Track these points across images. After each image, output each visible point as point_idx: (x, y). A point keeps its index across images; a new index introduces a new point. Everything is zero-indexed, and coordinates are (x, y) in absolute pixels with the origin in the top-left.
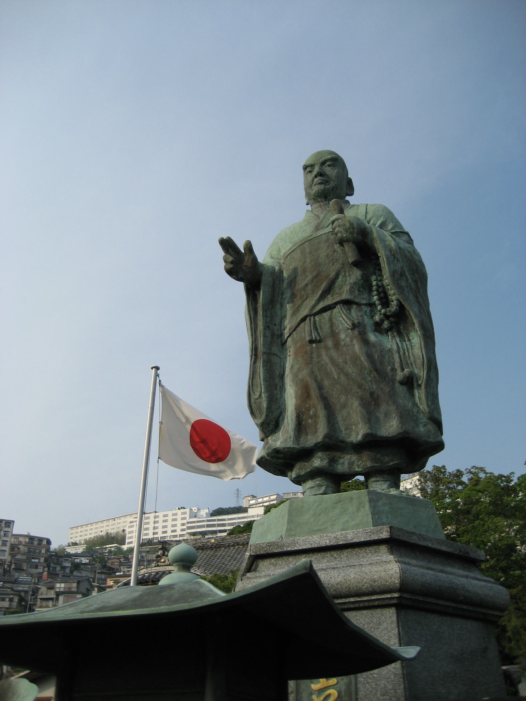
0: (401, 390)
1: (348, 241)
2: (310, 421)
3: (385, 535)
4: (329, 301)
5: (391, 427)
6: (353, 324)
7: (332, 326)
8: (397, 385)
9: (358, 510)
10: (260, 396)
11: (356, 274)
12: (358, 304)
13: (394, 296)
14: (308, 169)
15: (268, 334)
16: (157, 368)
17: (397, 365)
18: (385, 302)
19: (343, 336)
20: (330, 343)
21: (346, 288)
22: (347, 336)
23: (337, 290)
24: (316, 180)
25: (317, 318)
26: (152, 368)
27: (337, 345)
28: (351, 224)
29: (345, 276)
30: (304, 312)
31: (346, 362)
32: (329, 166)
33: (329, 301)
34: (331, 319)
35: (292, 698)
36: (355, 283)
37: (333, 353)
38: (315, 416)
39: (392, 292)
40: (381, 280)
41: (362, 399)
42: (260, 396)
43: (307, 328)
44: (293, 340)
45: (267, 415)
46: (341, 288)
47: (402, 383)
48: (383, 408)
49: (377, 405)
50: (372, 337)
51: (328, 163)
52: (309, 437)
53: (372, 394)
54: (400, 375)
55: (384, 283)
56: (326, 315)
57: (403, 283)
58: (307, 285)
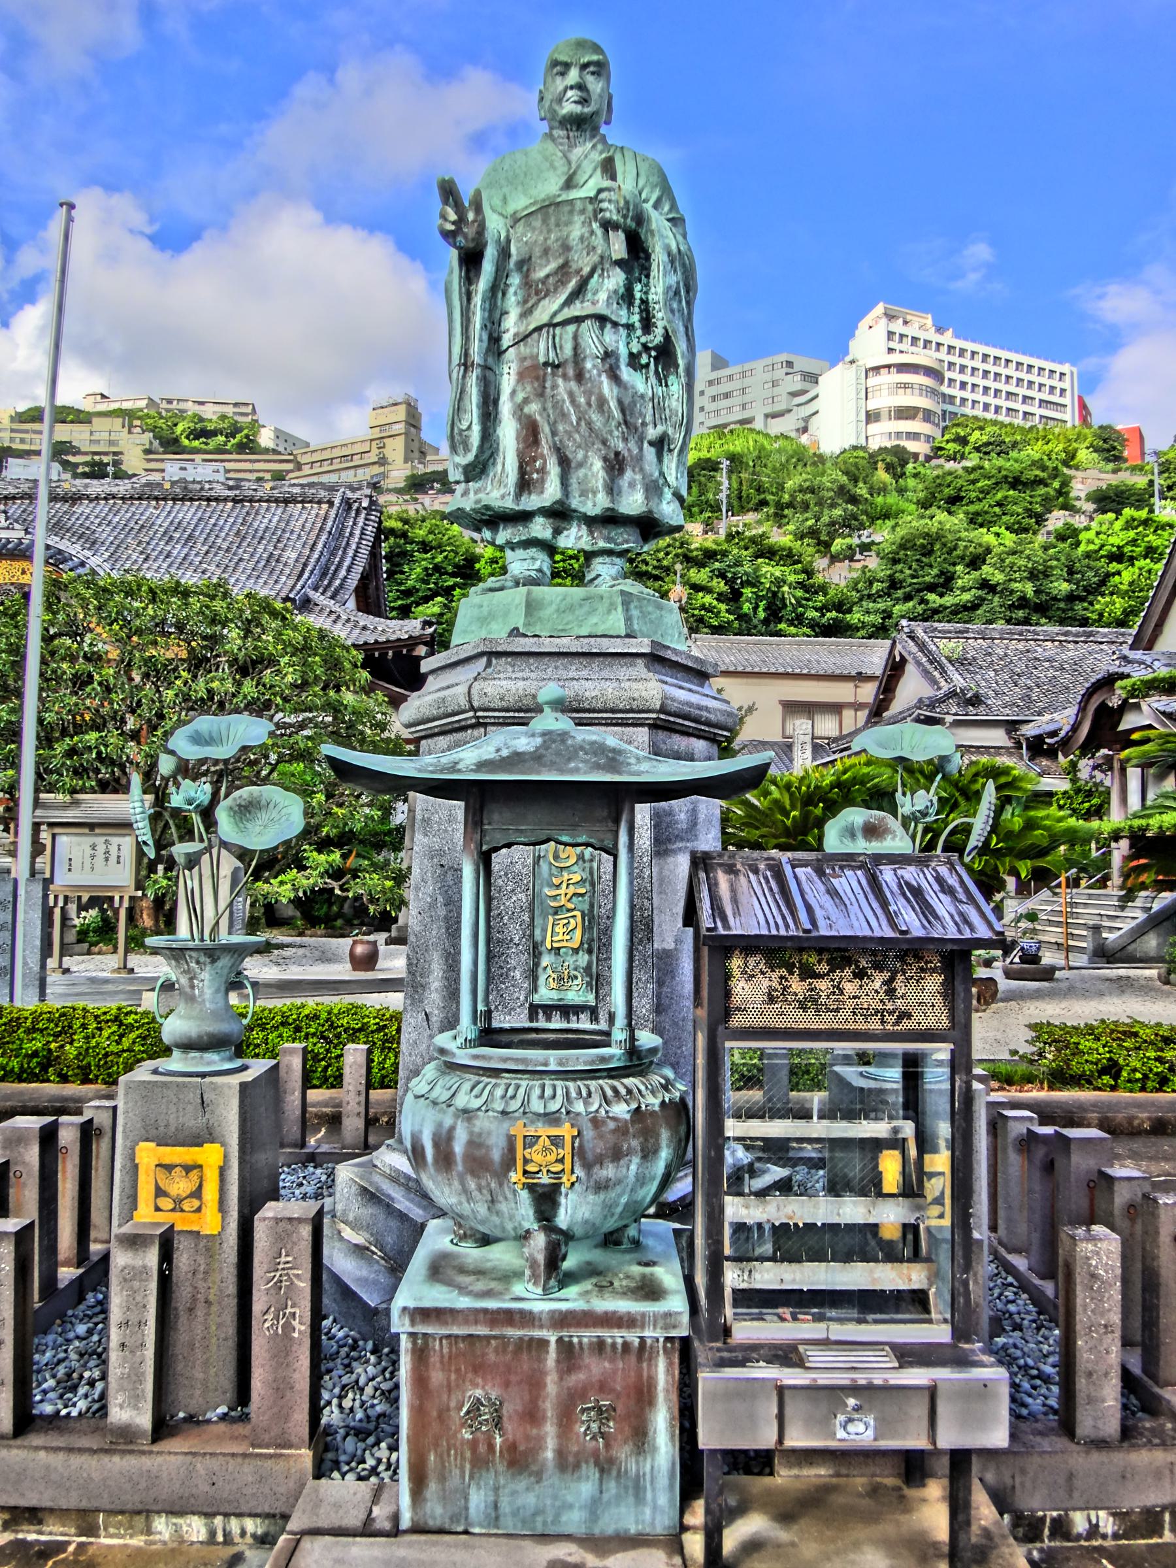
0: (650, 453)
1: (616, 226)
2: (535, 476)
3: (647, 650)
4: (576, 310)
5: (633, 503)
6: (606, 353)
7: (576, 348)
8: (646, 445)
9: (609, 612)
10: (469, 428)
11: (616, 279)
12: (615, 324)
13: (661, 318)
14: (558, 68)
15: (485, 337)
16: (72, 207)
17: (649, 418)
18: (647, 324)
19: (588, 365)
20: (571, 372)
21: (602, 296)
22: (594, 366)
23: (589, 296)
24: (570, 93)
25: (558, 330)
26: (61, 205)
27: (580, 377)
28: (627, 203)
29: (602, 275)
30: (541, 315)
31: (589, 404)
32: (593, 73)
33: (576, 310)
34: (575, 337)
35: (1169, 819)
36: (616, 292)
37: (573, 385)
38: (543, 471)
39: (660, 315)
40: (646, 293)
41: (605, 459)
42: (469, 428)
43: (542, 345)
44: (518, 354)
45: (476, 456)
46: (595, 293)
47: (651, 443)
48: (628, 475)
49: (621, 471)
50: (626, 373)
51: (592, 69)
52: (533, 497)
53: (617, 454)
54: (652, 433)
55: (650, 297)
56: (571, 328)
57: (675, 305)
58: (548, 276)
